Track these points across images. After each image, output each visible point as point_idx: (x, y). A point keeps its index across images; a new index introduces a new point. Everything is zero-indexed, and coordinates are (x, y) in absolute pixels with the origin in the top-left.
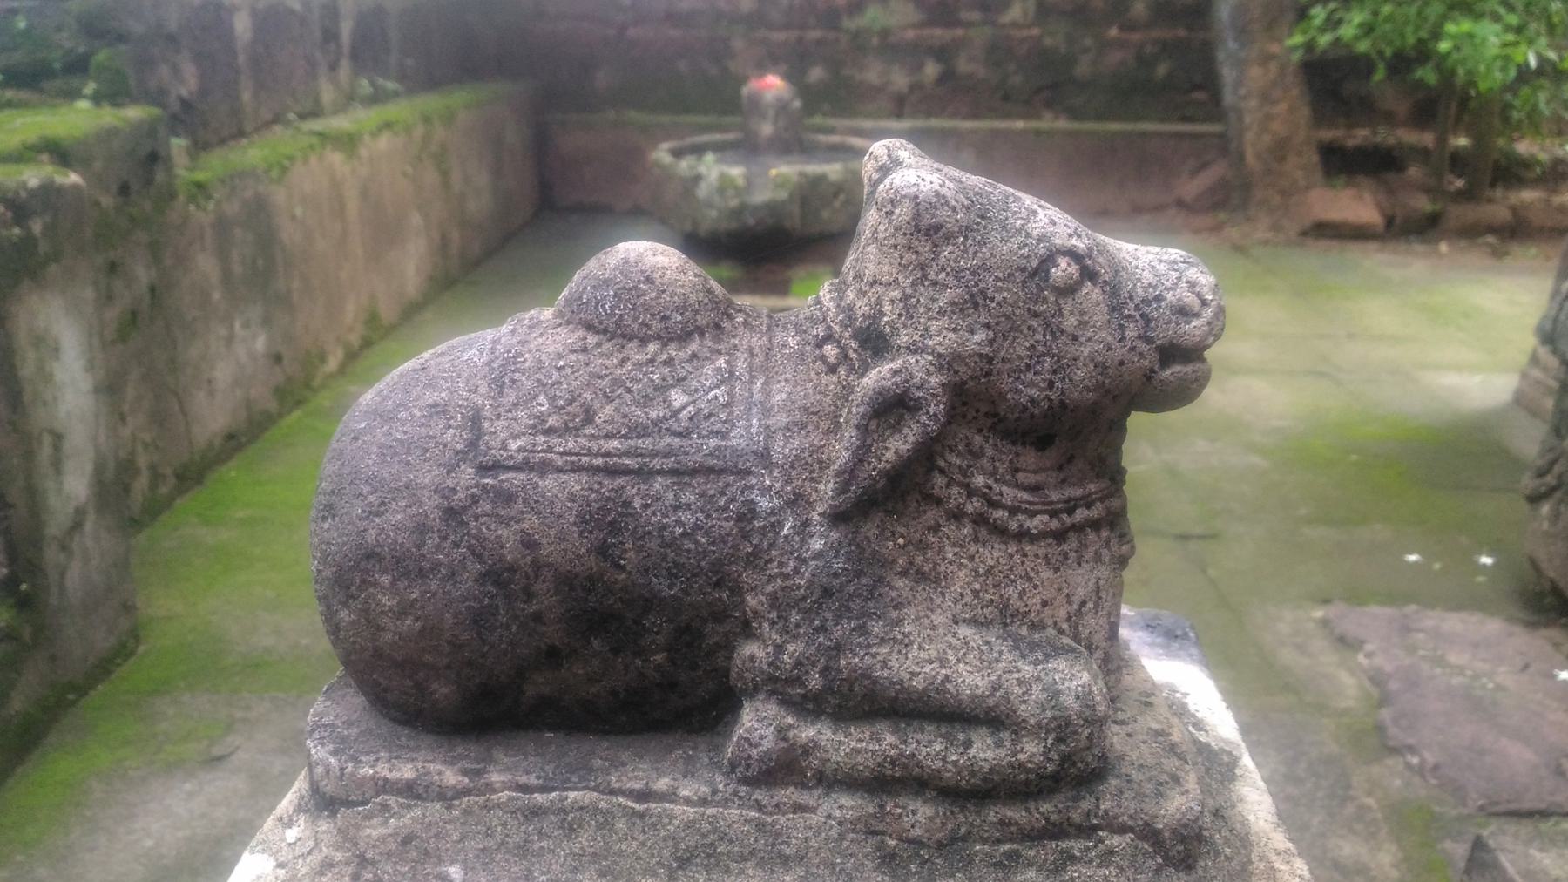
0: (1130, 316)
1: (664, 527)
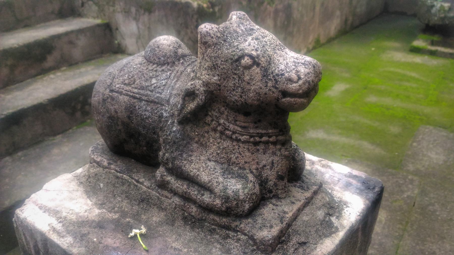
0: (270, 79)
1: (142, 115)
